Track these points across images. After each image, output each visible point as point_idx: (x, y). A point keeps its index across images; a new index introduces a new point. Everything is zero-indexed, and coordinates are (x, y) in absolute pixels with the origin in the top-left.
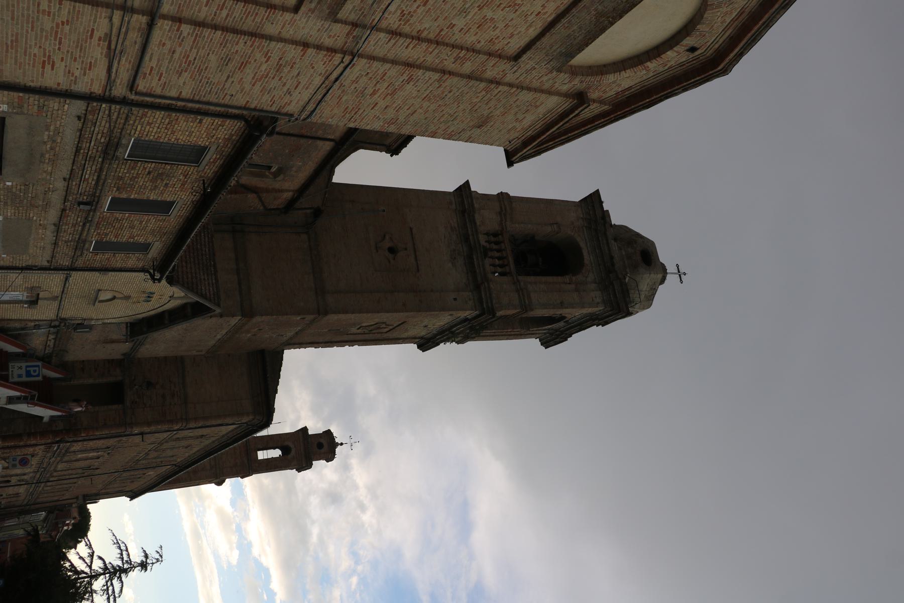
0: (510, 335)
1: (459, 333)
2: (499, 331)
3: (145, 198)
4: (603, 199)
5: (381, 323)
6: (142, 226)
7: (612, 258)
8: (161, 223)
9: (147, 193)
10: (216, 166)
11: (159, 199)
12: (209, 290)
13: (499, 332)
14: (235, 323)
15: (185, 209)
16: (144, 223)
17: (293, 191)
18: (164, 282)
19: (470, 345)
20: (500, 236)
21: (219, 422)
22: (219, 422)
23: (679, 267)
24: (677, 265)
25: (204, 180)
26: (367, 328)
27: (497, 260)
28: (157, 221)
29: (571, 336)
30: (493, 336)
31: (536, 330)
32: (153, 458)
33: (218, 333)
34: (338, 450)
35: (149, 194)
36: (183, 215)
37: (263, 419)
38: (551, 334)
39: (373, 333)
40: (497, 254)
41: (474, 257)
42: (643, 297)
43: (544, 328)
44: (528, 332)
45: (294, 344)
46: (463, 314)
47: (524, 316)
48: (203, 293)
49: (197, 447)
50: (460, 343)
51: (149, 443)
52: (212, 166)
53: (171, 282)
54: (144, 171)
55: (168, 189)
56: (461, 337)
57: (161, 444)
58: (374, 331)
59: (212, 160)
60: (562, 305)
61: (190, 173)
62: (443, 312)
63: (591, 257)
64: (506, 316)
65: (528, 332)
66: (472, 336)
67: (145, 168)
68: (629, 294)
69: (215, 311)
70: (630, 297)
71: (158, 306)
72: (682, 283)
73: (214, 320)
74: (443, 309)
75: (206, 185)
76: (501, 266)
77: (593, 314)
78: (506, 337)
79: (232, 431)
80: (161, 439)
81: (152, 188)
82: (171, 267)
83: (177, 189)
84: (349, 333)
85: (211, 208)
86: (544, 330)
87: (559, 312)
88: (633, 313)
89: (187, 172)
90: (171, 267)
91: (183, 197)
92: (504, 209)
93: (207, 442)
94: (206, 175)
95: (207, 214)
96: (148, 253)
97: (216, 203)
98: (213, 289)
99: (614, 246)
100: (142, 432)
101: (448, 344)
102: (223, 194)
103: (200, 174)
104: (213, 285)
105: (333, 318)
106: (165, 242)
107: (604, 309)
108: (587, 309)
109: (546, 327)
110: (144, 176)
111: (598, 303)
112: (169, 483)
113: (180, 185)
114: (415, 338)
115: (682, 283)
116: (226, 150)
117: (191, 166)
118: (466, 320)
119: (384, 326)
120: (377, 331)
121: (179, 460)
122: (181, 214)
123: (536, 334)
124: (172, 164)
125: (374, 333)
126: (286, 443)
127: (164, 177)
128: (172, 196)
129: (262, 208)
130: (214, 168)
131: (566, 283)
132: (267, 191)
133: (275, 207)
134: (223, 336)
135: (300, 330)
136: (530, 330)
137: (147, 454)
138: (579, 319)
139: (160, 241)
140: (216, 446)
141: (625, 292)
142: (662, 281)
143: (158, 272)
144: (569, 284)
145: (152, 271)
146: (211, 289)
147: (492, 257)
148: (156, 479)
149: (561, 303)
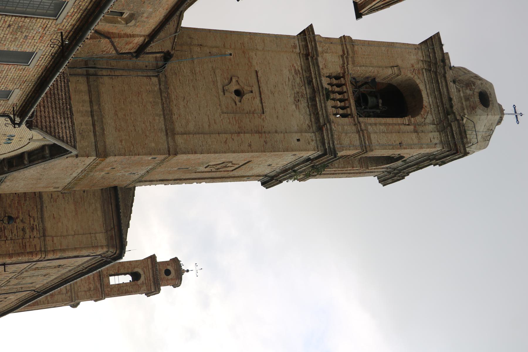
0: (349, 173)
1: (301, 172)
2: (339, 169)
3: (6, 49)
4: (443, 42)
5: (228, 162)
6: (3, 75)
7: (450, 99)
8: (21, 72)
9: (7, 45)
10: (73, 19)
11: (19, 50)
12: (66, 132)
13: (339, 171)
14: (89, 163)
15: (44, 59)
16: (5, 72)
17: (144, 36)
18: (24, 126)
19: (312, 182)
20: (342, 79)
21: (75, 254)
22: (75, 254)
23: (516, 108)
24: (514, 105)
25: (62, 33)
26: (215, 167)
27: (338, 102)
28: (17, 70)
29: (408, 175)
30: (334, 174)
31: (375, 169)
32: (14, 285)
33: (74, 172)
34: (185, 276)
35: (9, 46)
36: (41, 65)
37: (116, 252)
38: (389, 173)
39: (219, 171)
40: (339, 97)
41: (317, 99)
42: (479, 137)
43: (382, 167)
44: (367, 171)
45: (146, 181)
46: (305, 155)
47: (363, 156)
48: (60, 136)
49: (54, 275)
50: (302, 181)
51: (10, 272)
52: (69, 20)
53: (30, 126)
54: (5, 24)
55: (27, 41)
56: (303, 175)
57: (21, 272)
58: (220, 170)
59: (69, 14)
60: (400, 146)
61: (48, 26)
62: (287, 153)
63: (430, 99)
64: (347, 156)
65: (367, 171)
66: (314, 174)
67: (5, 22)
68: (466, 134)
69: (71, 152)
70: (467, 138)
71: (18, 147)
72: (518, 123)
73: (70, 160)
74: (287, 150)
75: (64, 37)
76: (343, 108)
77: (430, 154)
78: (346, 175)
79: (87, 261)
80: (21, 269)
81: (13, 40)
82: (31, 113)
83: (36, 41)
84: (197, 171)
85: (69, 59)
86: (382, 168)
87: (396, 152)
88: (469, 153)
89: (46, 25)
90: (31, 113)
91: (41, 48)
92: (346, 52)
93: (64, 271)
94: (64, 27)
95: (65, 65)
96: (8, 100)
97: (74, 55)
98: (70, 132)
99: (453, 88)
100: (4, 263)
101: (290, 181)
102: (80, 46)
103: (58, 27)
104: (69, 128)
105: (182, 158)
106: (24, 89)
107: (441, 149)
108: (425, 149)
109: (385, 166)
110: (5, 29)
111: (436, 144)
112: (29, 306)
113: (39, 37)
114: (259, 176)
115: (518, 123)
116: (84, 4)
117: (50, 19)
118: (308, 159)
119: (230, 165)
120: (224, 169)
121: (37, 286)
122: (40, 64)
123: (375, 172)
124: (31, 18)
125: (221, 171)
126: (136, 270)
127: (24, 30)
128: (31, 48)
129: (114, 52)
130: (72, 21)
131: (405, 125)
132: (120, 36)
133: (126, 52)
134: (78, 174)
135: (151, 169)
136: (369, 168)
137: (9, 281)
138: (416, 159)
139: (20, 88)
140: (72, 275)
141: (463, 134)
142: (499, 122)
143: (18, 116)
144: (408, 125)
145: (12, 116)
146: (68, 132)
147: (333, 99)
148: (16, 302)
149: (400, 144)
